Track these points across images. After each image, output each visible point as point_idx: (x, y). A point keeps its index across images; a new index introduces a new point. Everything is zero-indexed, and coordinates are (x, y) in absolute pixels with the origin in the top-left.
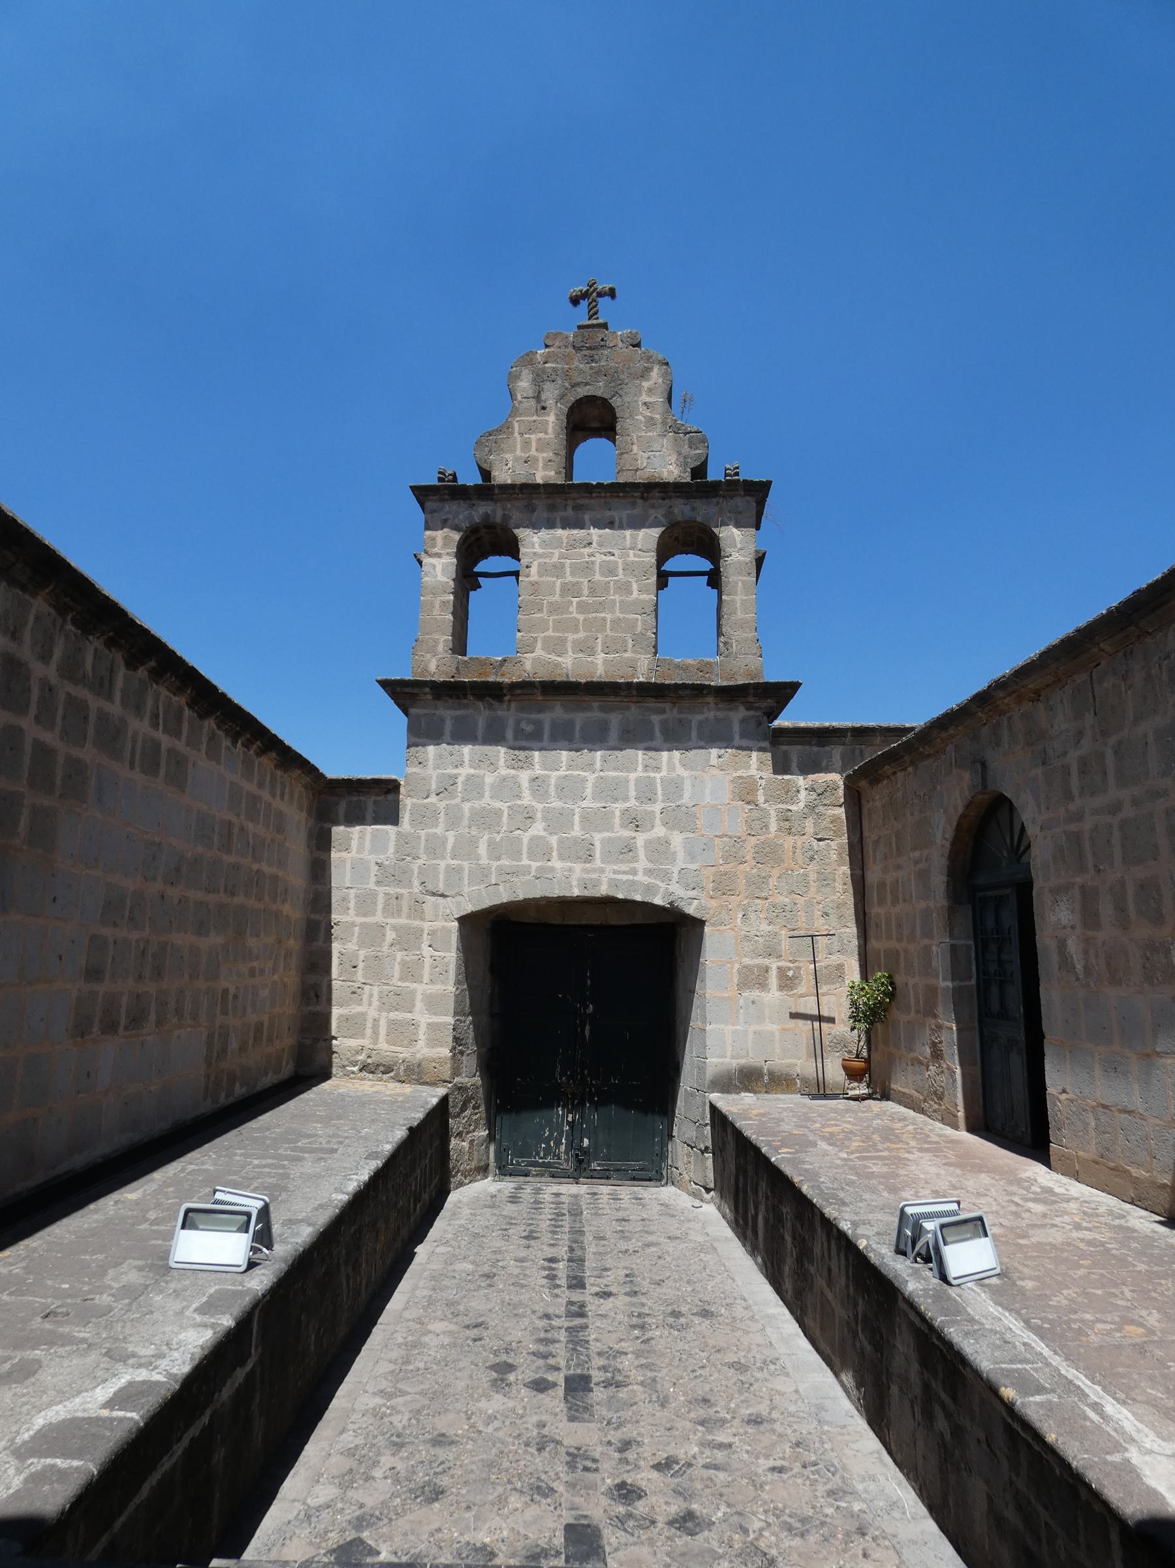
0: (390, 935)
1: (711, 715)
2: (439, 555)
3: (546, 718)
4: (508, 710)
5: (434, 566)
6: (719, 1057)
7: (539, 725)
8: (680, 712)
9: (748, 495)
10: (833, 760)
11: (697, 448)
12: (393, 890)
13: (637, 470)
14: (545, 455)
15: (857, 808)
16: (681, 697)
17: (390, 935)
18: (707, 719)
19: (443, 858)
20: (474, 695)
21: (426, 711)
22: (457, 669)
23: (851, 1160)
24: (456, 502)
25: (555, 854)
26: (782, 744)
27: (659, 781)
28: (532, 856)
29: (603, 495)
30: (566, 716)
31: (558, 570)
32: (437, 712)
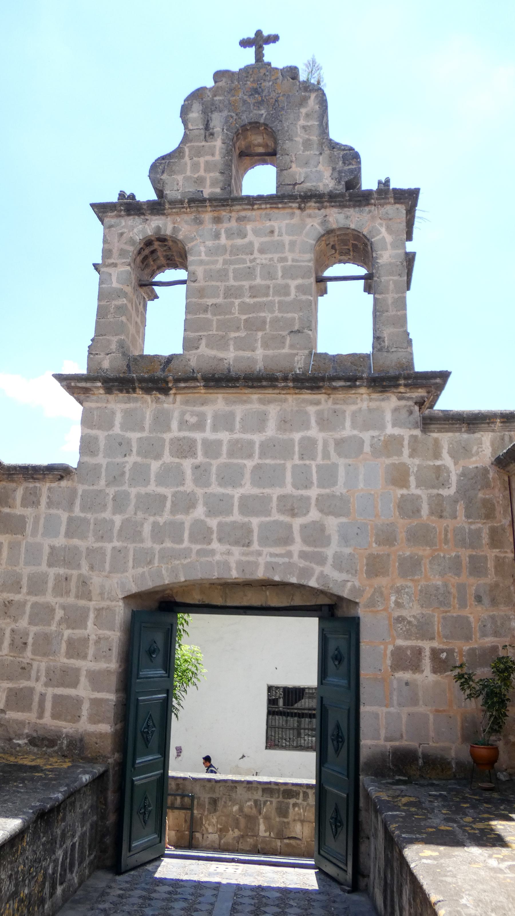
0: (59, 614)
1: (364, 405)
2: (115, 265)
3: (209, 410)
4: (174, 403)
5: (110, 275)
6: (373, 739)
7: (202, 417)
8: (335, 403)
9: (398, 203)
10: (484, 446)
11: (350, 164)
12: (62, 571)
13: (296, 184)
14: (212, 174)
15: (508, 492)
16: (335, 388)
17: (59, 614)
18: (360, 409)
19: (111, 541)
20: (142, 389)
21: (99, 405)
22: (128, 366)
23: (501, 871)
24: (131, 217)
25: (215, 536)
26: (434, 432)
27: (314, 470)
28: (193, 539)
29: (263, 206)
30: (227, 409)
31: (222, 275)
32: (109, 406)
